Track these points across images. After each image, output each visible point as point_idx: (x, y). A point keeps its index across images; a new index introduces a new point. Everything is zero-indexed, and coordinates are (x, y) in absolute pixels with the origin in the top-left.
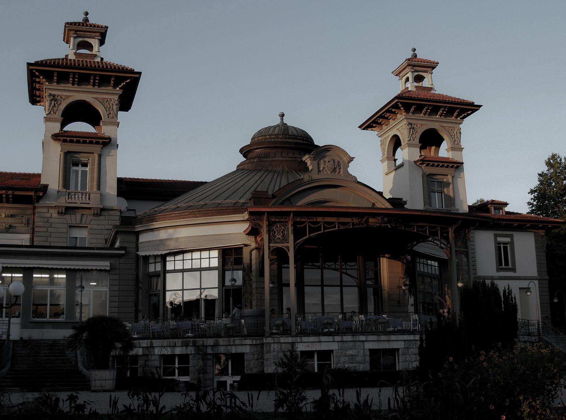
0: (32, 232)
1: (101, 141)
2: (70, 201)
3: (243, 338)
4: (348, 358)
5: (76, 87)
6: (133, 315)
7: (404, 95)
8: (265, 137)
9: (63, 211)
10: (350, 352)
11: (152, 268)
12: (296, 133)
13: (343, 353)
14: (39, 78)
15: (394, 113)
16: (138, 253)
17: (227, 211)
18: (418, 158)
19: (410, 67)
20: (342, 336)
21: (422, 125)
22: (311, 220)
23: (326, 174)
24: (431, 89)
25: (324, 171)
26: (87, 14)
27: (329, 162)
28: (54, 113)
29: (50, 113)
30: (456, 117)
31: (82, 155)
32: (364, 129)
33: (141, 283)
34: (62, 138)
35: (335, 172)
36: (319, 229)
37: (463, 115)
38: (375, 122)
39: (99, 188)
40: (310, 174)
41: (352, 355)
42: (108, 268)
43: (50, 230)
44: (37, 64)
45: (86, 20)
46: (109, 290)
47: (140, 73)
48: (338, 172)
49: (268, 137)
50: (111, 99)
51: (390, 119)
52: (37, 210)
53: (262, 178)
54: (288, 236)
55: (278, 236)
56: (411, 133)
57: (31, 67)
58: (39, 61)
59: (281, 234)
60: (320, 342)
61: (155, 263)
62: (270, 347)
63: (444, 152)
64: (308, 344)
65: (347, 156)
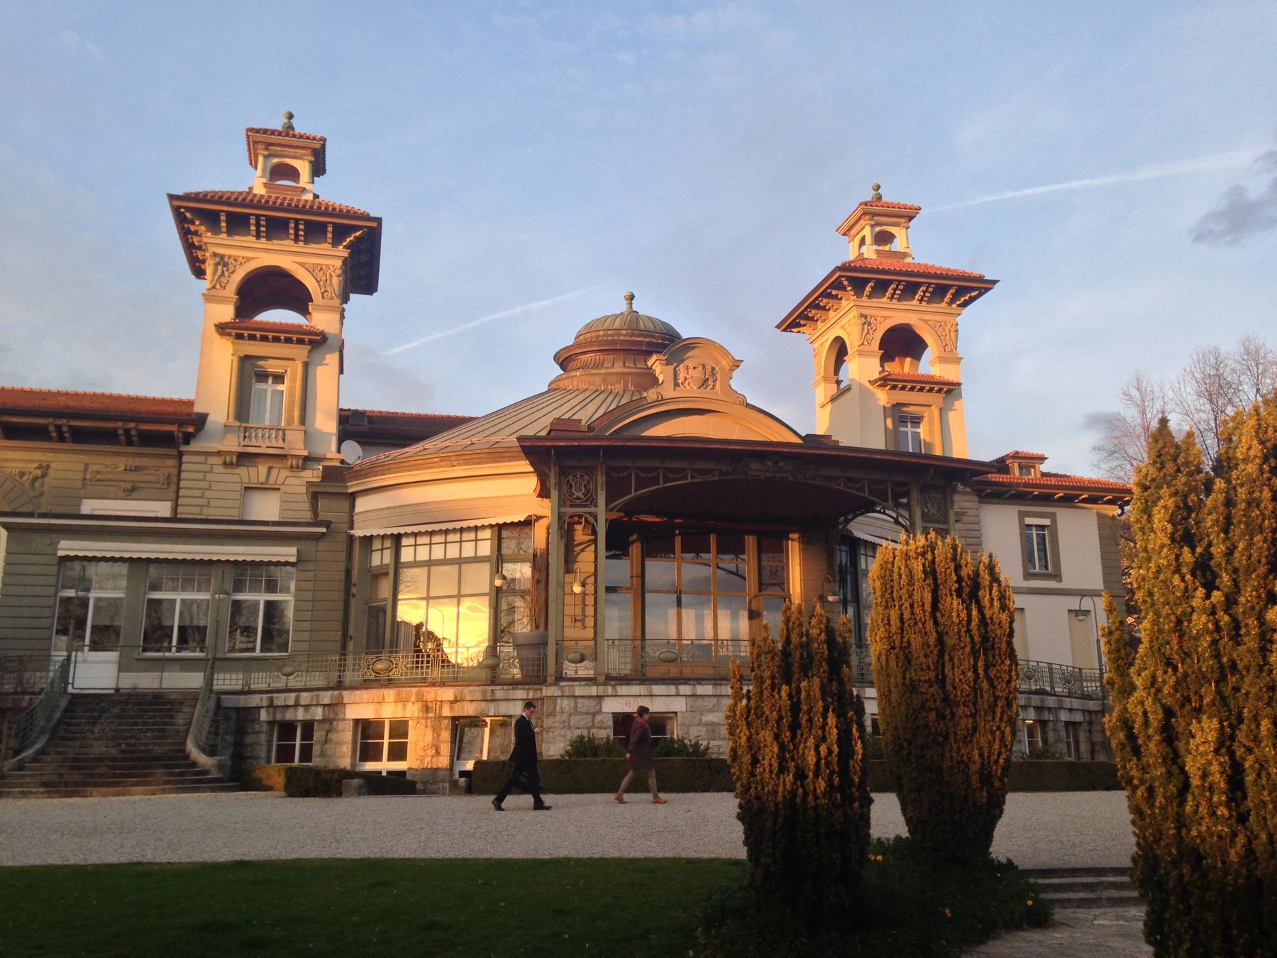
0: (174, 498)
1: (307, 338)
2: (247, 442)
3: (511, 687)
4: (705, 728)
5: (263, 243)
6: (338, 646)
7: (852, 265)
8: (596, 334)
9: (234, 461)
10: (708, 718)
11: (376, 560)
12: (651, 327)
13: (697, 719)
14: (193, 223)
15: (835, 297)
16: (352, 532)
17: (508, 454)
18: (877, 376)
19: (867, 217)
20: (694, 685)
21: (886, 318)
22: (638, 464)
23: (689, 391)
24: (905, 255)
25: (686, 384)
26: (291, 116)
27: (694, 368)
28: (221, 286)
29: (214, 287)
30: (950, 304)
31: (270, 362)
32: (785, 330)
33: (355, 585)
34: (234, 332)
35: (706, 387)
36: (655, 481)
37: (962, 299)
38: (803, 316)
39: (303, 421)
40: (659, 389)
41: (713, 724)
42: (293, 559)
43: (208, 494)
44: (187, 197)
45: (290, 127)
46: (295, 600)
47: (379, 220)
48: (711, 386)
49: (601, 333)
50: (328, 266)
51: (829, 310)
52: (185, 458)
53: (584, 403)
54: (596, 494)
55: (577, 494)
56: (866, 331)
57: (176, 203)
58: (191, 193)
59: (584, 490)
60: (651, 696)
61: (382, 549)
62: (555, 704)
63: (929, 365)
64: (627, 699)
65: (728, 357)
